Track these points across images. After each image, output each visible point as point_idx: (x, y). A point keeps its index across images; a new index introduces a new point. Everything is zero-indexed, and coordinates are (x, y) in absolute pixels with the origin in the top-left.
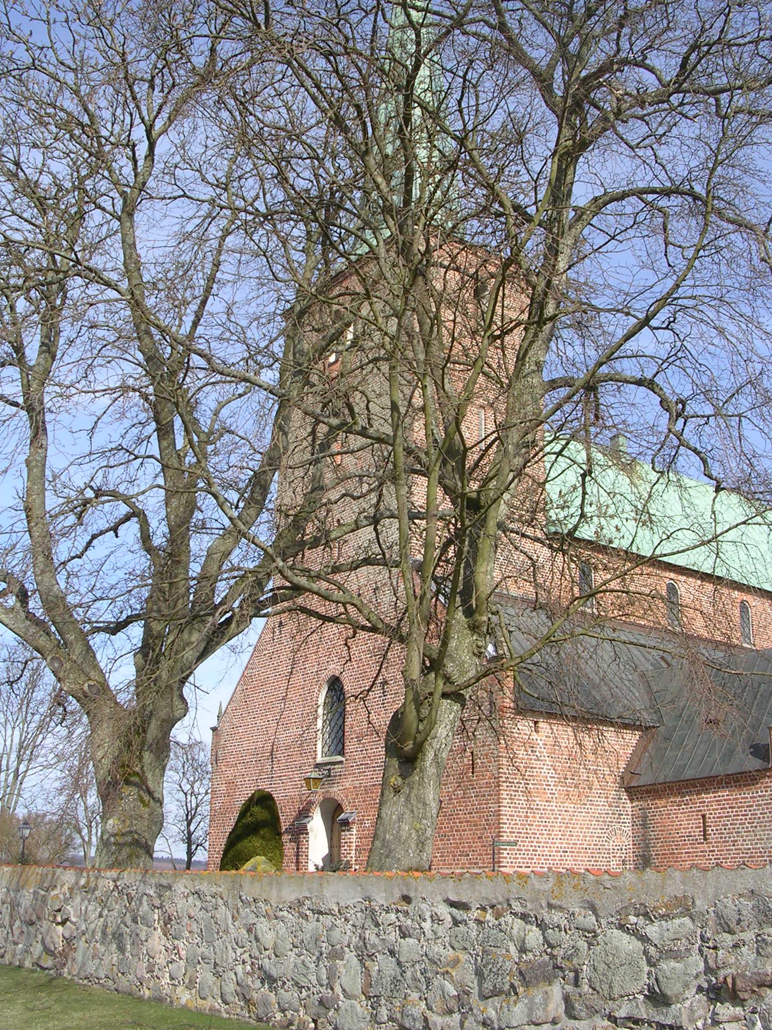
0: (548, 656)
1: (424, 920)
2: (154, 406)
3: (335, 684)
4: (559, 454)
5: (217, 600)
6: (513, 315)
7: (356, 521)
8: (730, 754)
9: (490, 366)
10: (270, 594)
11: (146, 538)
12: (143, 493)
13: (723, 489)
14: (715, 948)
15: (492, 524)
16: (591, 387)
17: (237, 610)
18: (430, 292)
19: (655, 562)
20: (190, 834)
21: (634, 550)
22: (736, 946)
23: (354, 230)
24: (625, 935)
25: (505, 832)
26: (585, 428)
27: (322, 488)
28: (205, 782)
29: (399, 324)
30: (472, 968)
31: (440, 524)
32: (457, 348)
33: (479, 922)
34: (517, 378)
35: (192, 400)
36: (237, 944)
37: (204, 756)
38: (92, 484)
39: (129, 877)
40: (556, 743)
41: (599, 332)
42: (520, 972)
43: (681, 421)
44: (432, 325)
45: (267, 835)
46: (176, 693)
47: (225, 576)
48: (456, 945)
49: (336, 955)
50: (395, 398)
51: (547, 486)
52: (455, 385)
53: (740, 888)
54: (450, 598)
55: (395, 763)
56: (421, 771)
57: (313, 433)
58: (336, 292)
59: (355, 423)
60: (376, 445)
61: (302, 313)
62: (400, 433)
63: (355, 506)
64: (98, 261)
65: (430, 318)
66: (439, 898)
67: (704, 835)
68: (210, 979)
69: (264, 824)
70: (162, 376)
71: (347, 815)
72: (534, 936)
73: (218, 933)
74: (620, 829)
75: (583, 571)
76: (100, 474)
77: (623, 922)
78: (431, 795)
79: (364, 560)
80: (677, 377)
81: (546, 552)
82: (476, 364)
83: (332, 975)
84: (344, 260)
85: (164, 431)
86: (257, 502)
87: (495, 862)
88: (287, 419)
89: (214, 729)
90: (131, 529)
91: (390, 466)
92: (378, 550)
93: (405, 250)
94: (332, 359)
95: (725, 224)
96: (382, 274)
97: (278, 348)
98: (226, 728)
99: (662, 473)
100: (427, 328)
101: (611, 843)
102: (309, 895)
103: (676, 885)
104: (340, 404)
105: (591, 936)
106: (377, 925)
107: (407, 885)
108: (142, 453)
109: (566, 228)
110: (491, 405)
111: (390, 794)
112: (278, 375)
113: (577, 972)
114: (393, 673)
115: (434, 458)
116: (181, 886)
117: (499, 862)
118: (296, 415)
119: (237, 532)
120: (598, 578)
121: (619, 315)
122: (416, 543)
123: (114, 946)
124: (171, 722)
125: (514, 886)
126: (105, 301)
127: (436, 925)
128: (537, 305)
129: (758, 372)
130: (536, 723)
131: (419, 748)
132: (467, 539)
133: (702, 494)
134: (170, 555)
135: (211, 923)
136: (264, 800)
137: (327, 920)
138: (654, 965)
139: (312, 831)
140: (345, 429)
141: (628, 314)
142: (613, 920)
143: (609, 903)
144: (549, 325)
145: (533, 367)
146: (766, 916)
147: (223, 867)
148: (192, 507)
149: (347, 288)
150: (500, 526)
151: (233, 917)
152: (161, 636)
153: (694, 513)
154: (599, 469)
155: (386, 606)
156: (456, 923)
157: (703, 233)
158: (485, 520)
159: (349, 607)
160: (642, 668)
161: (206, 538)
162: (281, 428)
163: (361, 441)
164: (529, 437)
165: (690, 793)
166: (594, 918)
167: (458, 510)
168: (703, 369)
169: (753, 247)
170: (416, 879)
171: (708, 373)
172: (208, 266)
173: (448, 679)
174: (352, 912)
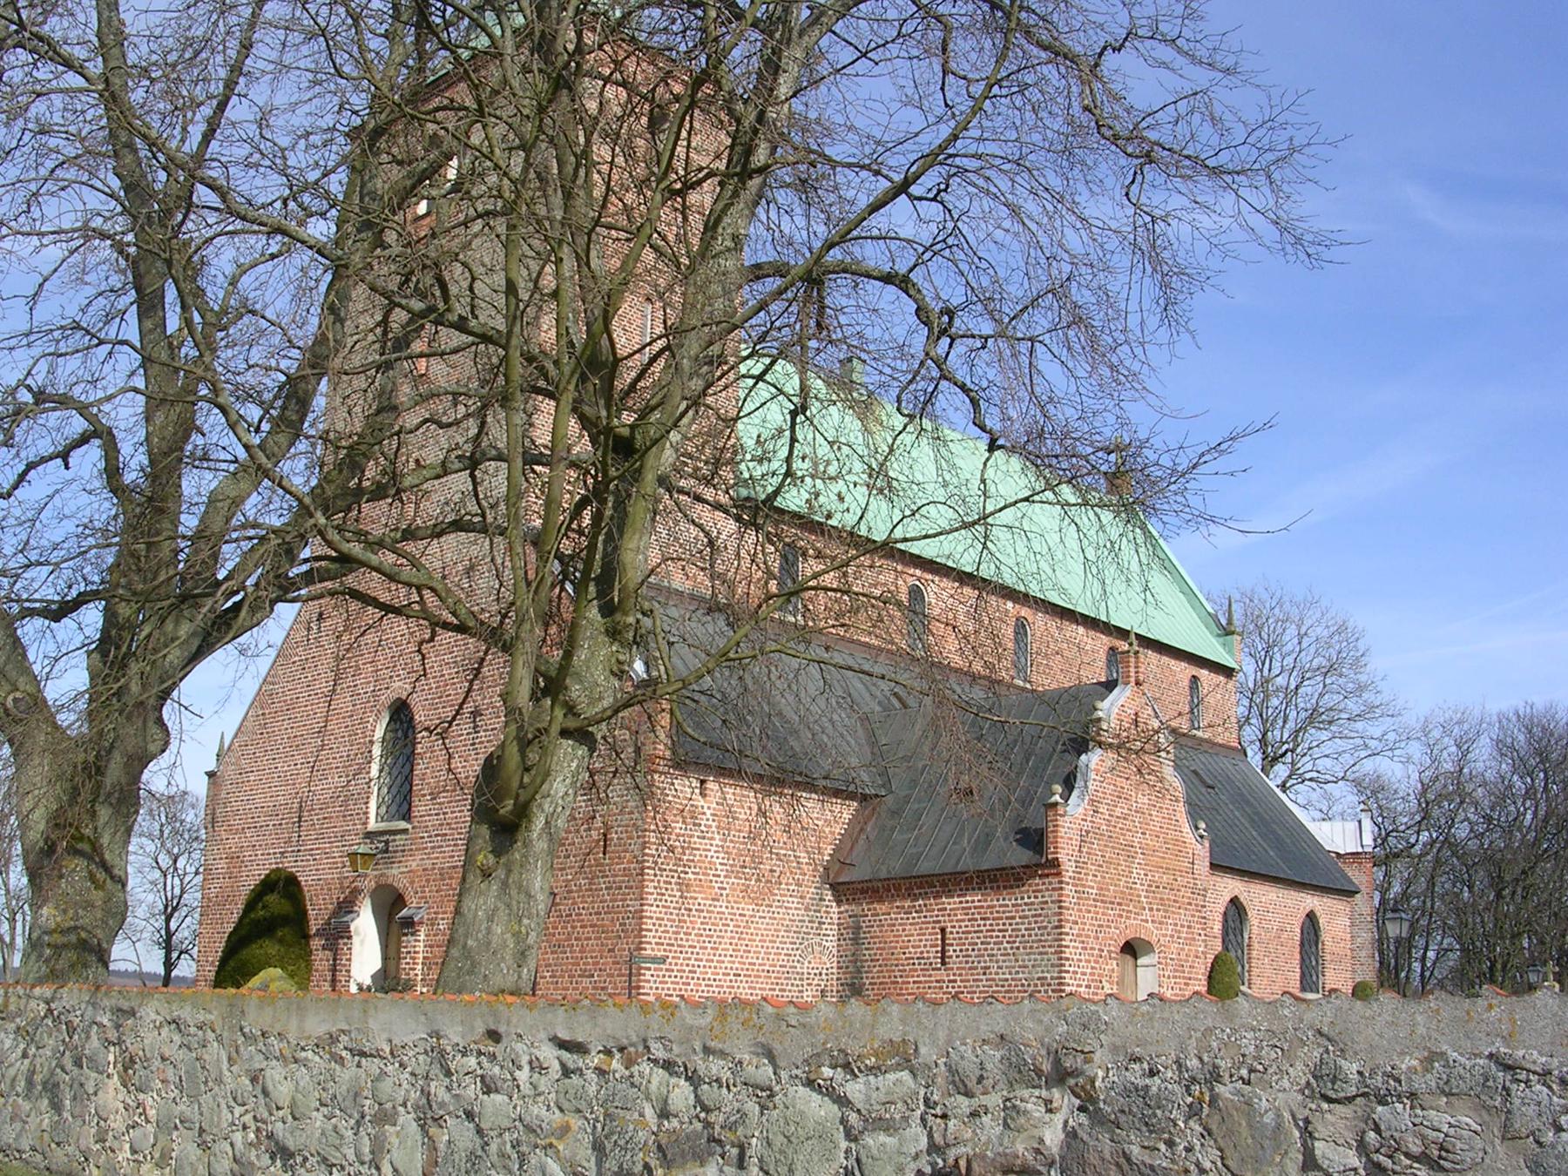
0: (721, 681)
1: (520, 1068)
2: (134, 264)
3: (401, 712)
4: (760, 378)
5: (220, 577)
6: (700, 160)
7: (443, 463)
8: (985, 841)
9: (664, 239)
10: (305, 568)
11: (112, 471)
12: (109, 398)
13: (1000, 447)
14: (944, 1116)
15: (650, 477)
16: (814, 279)
17: (250, 590)
18: (579, 115)
19: (888, 550)
20: (169, 935)
21: (863, 532)
22: (974, 1114)
23: (468, 10)
24: (814, 1094)
26: (801, 341)
27: (395, 408)
28: (196, 855)
29: (526, 160)
30: (587, 1140)
31: (573, 474)
32: (615, 205)
33: (601, 1072)
34: (703, 257)
35: (195, 258)
36: (235, 1099)
37: (192, 817)
38: (29, 381)
39: (72, 996)
40: (731, 814)
41: (832, 198)
42: (660, 1147)
43: (945, 341)
44: (578, 165)
45: (289, 938)
46: (152, 716)
47: (234, 535)
48: (566, 1105)
49: (385, 1117)
50: (513, 275)
51: (740, 425)
52: (608, 257)
53: (985, 1030)
54: (580, 587)
55: (485, 831)
56: (525, 845)
57: (385, 322)
58: (436, 102)
59: (448, 310)
60: (482, 347)
61: (378, 133)
62: (517, 329)
63: (444, 438)
64: (54, 27)
65: (575, 155)
66: (543, 1035)
67: (943, 958)
68: (193, 1152)
69: (284, 920)
70: (149, 217)
71: (412, 911)
72: (681, 1095)
73: (206, 1083)
75: (784, 557)
76: (43, 366)
77: (812, 1077)
78: (538, 882)
79: (454, 523)
80: (944, 273)
81: (732, 525)
82: (639, 233)
83: (379, 1147)
84: (448, 53)
85: (149, 306)
86: (290, 424)
87: (633, 989)
88: (344, 297)
89: (211, 775)
90: (90, 458)
91: (501, 380)
92: (476, 509)
93: (544, 45)
94: (422, 208)
95: (1035, 51)
96: (505, 81)
97: (337, 184)
98: (229, 772)
99: (911, 417)
100: (570, 169)
102: (346, 1027)
103: (892, 1023)
104: (428, 279)
105: (766, 1095)
106: (448, 1073)
107: (495, 1014)
108: (112, 335)
109: (795, 33)
110: (661, 296)
111: (474, 879)
112: (334, 228)
113: (742, 1149)
114: (488, 698)
115: (567, 370)
116: (151, 1012)
117: (639, 987)
118: (360, 293)
119: (258, 468)
120: (808, 567)
121: (864, 174)
122: (534, 502)
123: (44, 1103)
124: (144, 760)
125: (655, 1020)
126: (61, 91)
127: (536, 1076)
128: (742, 149)
129: (1065, 276)
130: (703, 782)
131: (523, 812)
132: (611, 498)
133: (969, 453)
134: (150, 499)
135: (194, 1068)
136: (282, 886)
137: (372, 1065)
138: (856, 1140)
139: (358, 934)
140: (432, 317)
141: (877, 173)
142: (798, 1072)
143: (794, 1048)
144: (756, 182)
145: (729, 243)
146: (1020, 1072)
147: (219, 983)
148: (188, 427)
149: (452, 101)
150: (662, 481)
151: (230, 1059)
152: (133, 627)
153: (955, 480)
154: (817, 404)
155: (484, 596)
156: (566, 1072)
157: (1000, 59)
158: (639, 471)
159: (427, 594)
160: (866, 709)
161: (209, 475)
162: (334, 311)
163: (458, 339)
164: (715, 349)
165: (925, 896)
166: (770, 1070)
167: (599, 453)
168: (984, 265)
169: (1074, 89)
170: (509, 1005)
171: (991, 271)
172: (233, 44)
173: (571, 709)
174: (411, 1054)
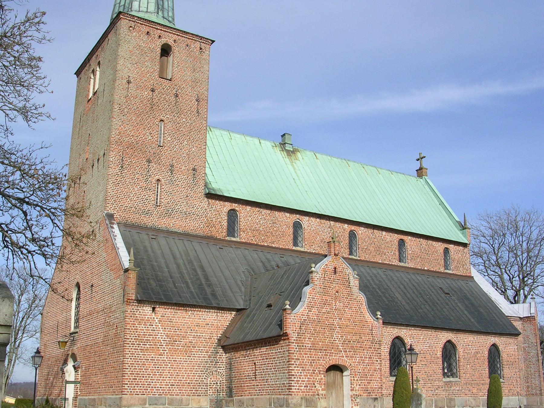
25: (127, 374)
74: (216, 371)
101: (209, 379)
139: (68, 372)
